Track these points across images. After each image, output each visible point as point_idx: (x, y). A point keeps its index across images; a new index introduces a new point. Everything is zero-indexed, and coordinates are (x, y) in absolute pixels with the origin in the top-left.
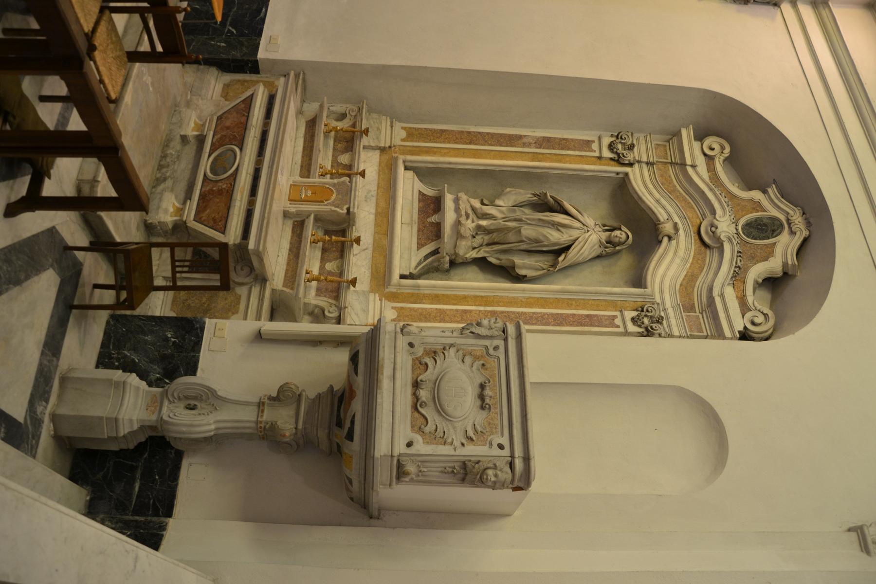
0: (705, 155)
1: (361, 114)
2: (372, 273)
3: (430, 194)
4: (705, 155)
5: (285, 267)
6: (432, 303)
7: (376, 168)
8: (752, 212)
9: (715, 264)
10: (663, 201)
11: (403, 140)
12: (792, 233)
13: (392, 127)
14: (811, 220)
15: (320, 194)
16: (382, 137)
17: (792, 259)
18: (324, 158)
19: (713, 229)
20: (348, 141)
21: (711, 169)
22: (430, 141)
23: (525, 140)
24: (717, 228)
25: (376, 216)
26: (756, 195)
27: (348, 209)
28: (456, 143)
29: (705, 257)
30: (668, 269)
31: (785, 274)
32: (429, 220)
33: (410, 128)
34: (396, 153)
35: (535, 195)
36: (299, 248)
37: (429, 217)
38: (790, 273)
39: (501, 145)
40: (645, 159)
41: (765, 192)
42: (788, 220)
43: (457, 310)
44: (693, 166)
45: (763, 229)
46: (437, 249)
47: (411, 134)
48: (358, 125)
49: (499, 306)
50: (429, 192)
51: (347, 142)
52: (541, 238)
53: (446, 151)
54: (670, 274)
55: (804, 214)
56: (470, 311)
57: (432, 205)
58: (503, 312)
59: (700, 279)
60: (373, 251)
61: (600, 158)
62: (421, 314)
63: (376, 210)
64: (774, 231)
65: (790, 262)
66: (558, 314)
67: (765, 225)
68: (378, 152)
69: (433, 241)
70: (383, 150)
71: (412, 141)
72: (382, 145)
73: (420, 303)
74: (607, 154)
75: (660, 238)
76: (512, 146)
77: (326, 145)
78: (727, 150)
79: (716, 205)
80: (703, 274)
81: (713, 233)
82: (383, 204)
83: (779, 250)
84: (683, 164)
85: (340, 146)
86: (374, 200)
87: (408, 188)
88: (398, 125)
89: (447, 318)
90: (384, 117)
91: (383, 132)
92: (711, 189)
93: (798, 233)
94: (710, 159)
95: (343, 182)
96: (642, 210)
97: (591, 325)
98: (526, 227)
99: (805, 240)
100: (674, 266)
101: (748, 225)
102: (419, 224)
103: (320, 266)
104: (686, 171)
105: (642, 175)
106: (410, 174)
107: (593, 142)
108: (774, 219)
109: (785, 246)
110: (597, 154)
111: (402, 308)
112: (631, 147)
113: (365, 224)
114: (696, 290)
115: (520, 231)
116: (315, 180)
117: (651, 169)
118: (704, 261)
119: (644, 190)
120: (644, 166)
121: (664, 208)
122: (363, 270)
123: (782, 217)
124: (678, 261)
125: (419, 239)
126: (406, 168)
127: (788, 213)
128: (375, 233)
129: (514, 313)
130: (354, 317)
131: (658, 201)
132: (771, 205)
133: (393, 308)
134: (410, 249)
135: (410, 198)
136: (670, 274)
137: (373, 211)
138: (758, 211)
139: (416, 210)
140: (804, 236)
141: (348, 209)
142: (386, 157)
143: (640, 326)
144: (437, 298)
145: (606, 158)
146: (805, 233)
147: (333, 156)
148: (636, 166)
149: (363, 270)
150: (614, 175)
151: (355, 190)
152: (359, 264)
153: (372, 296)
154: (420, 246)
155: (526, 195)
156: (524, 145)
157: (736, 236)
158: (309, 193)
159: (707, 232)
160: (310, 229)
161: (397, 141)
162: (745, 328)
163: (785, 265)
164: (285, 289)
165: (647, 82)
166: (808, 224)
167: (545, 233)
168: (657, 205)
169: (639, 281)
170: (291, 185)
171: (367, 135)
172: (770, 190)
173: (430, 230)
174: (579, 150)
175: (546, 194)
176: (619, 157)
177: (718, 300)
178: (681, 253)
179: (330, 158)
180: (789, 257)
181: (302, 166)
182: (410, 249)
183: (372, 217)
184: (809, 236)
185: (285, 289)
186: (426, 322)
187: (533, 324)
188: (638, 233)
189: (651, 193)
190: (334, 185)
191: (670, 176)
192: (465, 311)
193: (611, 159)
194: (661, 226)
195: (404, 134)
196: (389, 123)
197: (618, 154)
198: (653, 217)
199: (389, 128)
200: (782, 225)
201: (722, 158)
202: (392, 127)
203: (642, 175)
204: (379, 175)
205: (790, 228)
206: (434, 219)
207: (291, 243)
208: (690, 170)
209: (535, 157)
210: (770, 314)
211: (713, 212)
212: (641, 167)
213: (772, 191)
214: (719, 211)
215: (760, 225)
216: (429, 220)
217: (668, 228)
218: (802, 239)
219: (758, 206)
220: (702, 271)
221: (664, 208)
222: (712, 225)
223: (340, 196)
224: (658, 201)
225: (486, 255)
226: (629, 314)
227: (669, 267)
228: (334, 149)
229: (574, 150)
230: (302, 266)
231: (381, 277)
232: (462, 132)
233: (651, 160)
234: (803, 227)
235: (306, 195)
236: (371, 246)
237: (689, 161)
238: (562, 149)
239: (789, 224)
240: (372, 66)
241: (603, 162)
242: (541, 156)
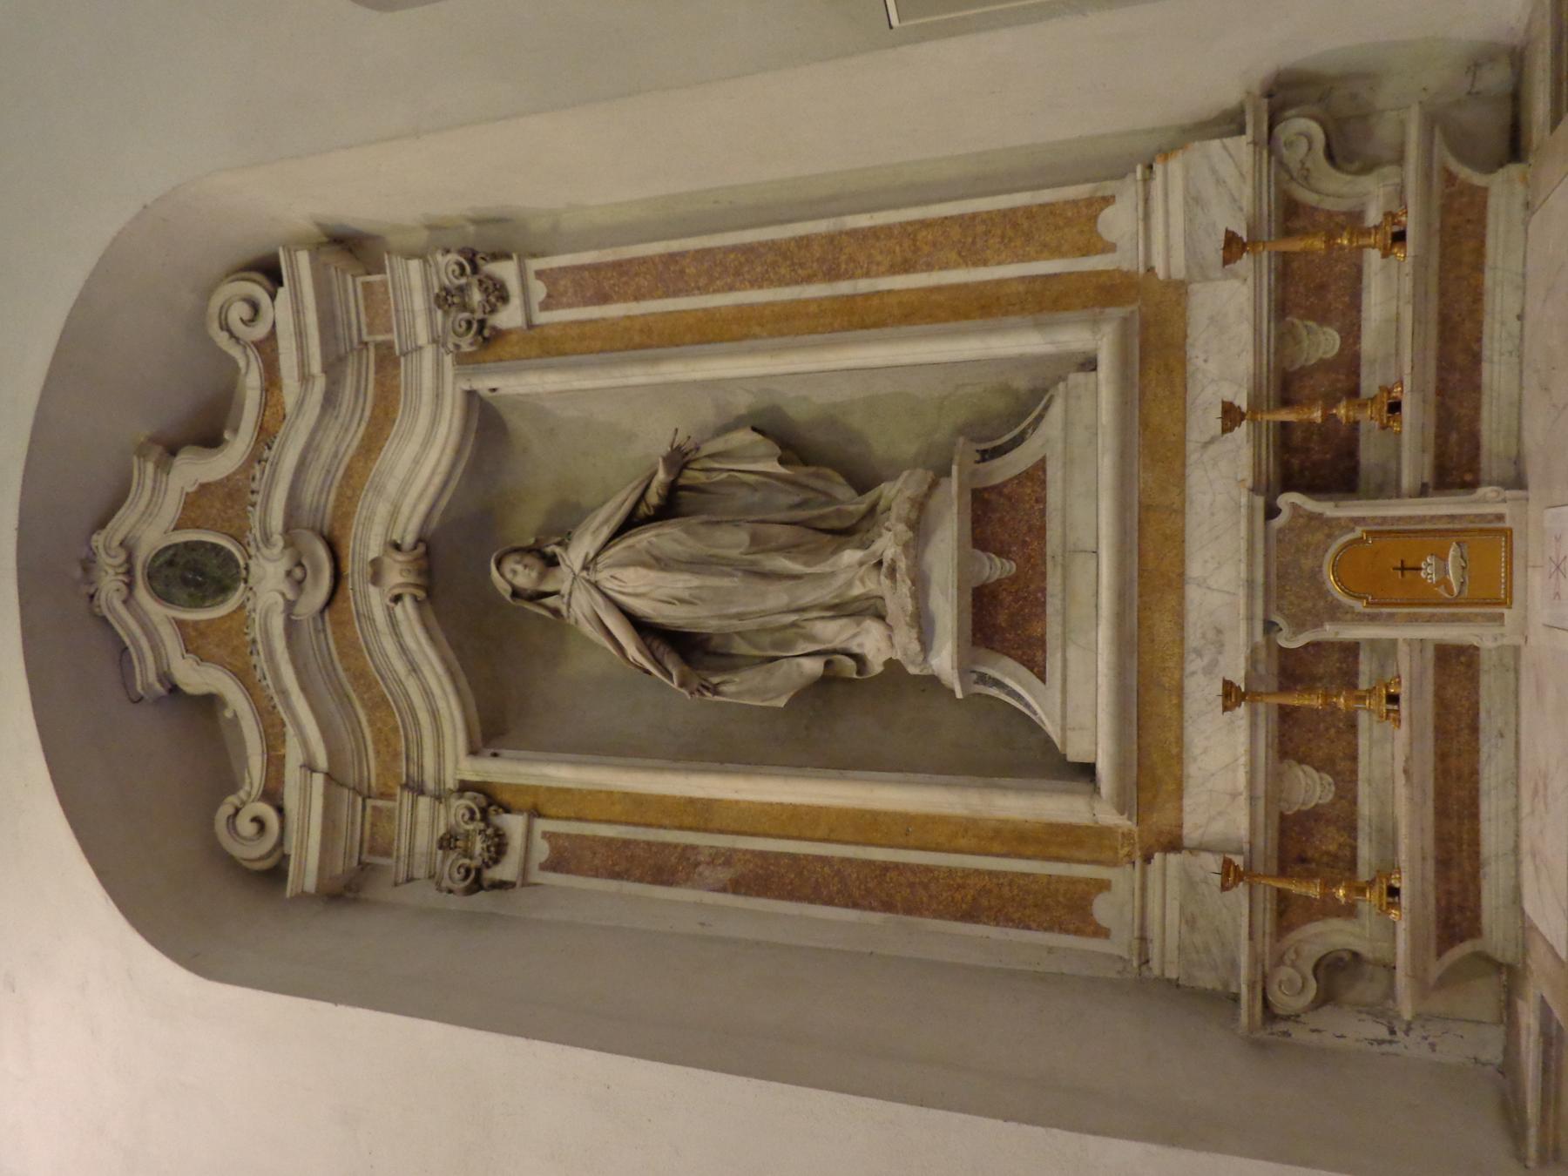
0: (280, 810)
1: (1256, 959)
2: (1183, 362)
3: (1011, 664)
4: (280, 810)
5: (1489, 279)
6: (1000, 283)
7: (1192, 769)
8: (210, 622)
9: (314, 480)
10: (400, 667)
11: (1103, 886)
12: (128, 547)
13: (1143, 939)
14: (78, 573)
15: (1389, 577)
16: (1174, 887)
17: (142, 472)
18: (1390, 761)
19: (298, 573)
20: (1302, 852)
21: (275, 763)
22: (1013, 878)
23: (724, 875)
24: (289, 574)
25: (1182, 575)
26: (195, 677)
27: (1272, 512)
28: (928, 869)
29: (336, 507)
30: (417, 462)
31: (172, 451)
32: (1010, 567)
33: (1078, 932)
34: (1127, 836)
35: (715, 690)
36: (1445, 365)
37: (1013, 579)
38: (159, 449)
39: (794, 858)
40: (424, 802)
41: (165, 677)
42: (130, 586)
43: (929, 267)
44: (309, 767)
45: (195, 574)
46: (983, 460)
47: (1070, 909)
48: (1266, 906)
49: (818, 301)
50: (1010, 674)
51: (1303, 860)
52: (702, 530)
53: (962, 842)
54: (412, 448)
55: (92, 597)
56: (894, 270)
57: (1004, 620)
58: (809, 279)
59: (355, 443)
60: (1182, 439)
61: (536, 813)
62: (1028, 237)
63: (1182, 598)
64: (171, 563)
65: (150, 467)
66: (676, 294)
67: (186, 582)
68: (1191, 833)
69: (998, 489)
70: (1174, 844)
71: (1073, 881)
72: (1173, 858)
73: (1033, 279)
74: (514, 824)
75: (421, 548)
76: (763, 855)
77: (1387, 839)
78: (225, 810)
79: (280, 644)
80: (347, 460)
81: (299, 564)
82: (1163, 625)
83: (171, 507)
84: (329, 777)
85: (1329, 841)
86: (1193, 638)
87: (1078, 697)
88: (1120, 944)
89: (955, 233)
90: (1172, 974)
91: (1173, 915)
92: (284, 693)
93: (115, 543)
94: (272, 795)
95: (1299, 626)
96: (457, 647)
97: (595, 268)
98: (734, 553)
99: (102, 524)
100: (401, 470)
101: (222, 589)
102: (1043, 555)
103: (1358, 338)
104: (331, 755)
105: (439, 755)
106: (1076, 752)
107: (544, 867)
108: (164, 597)
109: (153, 521)
110: (541, 825)
111: (1086, 252)
112: (447, 842)
113: (1220, 479)
114: (367, 413)
115: (755, 539)
116: (1409, 637)
117: (414, 769)
118: (340, 495)
119: (441, 704)
120: (430, 785)
121: (403, 649)
122: (1212, 368)
123: (143, 595)
124: (392, 487)
125: (1042, 500)
126: (1087, 771)
127: (125, 602)
128: (1181, 512)
129: (783, 282)
130: (1227, 170)
131: (414, 669)
132: (155, 624)
133: (1110, 248)
134: (1068, 463)
135: (1072, 653)
136: (412, 448)
137: (1193, 593)
138: (196, 623)
139: (1053, 605)
140: (104, 533)
141: (1272, 512)
142: (1161, 819)
143: (489, 277)
144: (982, 307)
145: (520, 811)
146: (98, 540)
147: (1354, 801)
148: (451, 784)
149: (1212, 368)
150: (505, 752)
151: (1250, 583)
152: (1226, 340)
153: (1179, 272)
154: (1036, 475)
155: (738, 688)
156: (726, 858)
157: (252, 551)
158: (1429, 572)
159: (317, 570)
160: (1411, 445)
161: (1122, 879)
162: (273, 297)
163: (164, 466)
164: (1478, 179)
165: (341, 1008)
166: (88, 565)
167: (691, 542)
168: (418, 658)
169: (486, 425)
170: (1507, 602)
171: (1228, 686)
172: (152, 677)
173: (1005, 519)
174: (582, 837)
175: (682, 685)
176: (484, 811)
177: (316, 366)
178: (383, 510)
179: (1363, 790)
180: (149, 483)
181: (1474, 729)
182: (1068, 463)
183: (1195, 569)
184: (93, 532)
185: (1478, 179)
186: (1014, 210)
187: (734, 249)
188: (473, 577)
189: (427, 693)
190: (1335, 612)
191: (378, 752)
192: (906, 267)
193: (507, 811)
194: (411, 579)
195: (1102, 909)
196: (1154, 952)
197: (485, 817)
198: (433, 621)
199: (1154, 931)
200: (151, 577)
201: (242, 794)
202: (1143, 939)
203: (439, 755)
204: (1180, 740)
205: (130, 559)
206: (995, 568)
207: (1477, 388)
208: (322, 761)
209: (701, 814)
210: (222, 339)
211: (291, 626)
212: (439, 781)
213: (146, 676)
214: (277, 624)
215: (198, 585)
216: (1010, 567)
217: (397, 575)
218: (110, 525)
219: (194, 640)
220: (349, 468)
221: (403, 649)
222: (299, 584)
223: (1307, 563)
224: (414, 669)
225: (859, 499)
226: (509, 317)
227: (416, 469)
228: (1352, 829)
229: (594, 839)
230: (1420, 263)
231: (1156, 351)
232: (909, 911)
233: (407, 797)
234: (103, 558)
235: (1442, 558)
236: (1192, 458)
237: (318, 780)
238: (626, 843)
239: (130, 572)
240: (1219, 1148)
241: (528, 800)
242: (688, 820)
